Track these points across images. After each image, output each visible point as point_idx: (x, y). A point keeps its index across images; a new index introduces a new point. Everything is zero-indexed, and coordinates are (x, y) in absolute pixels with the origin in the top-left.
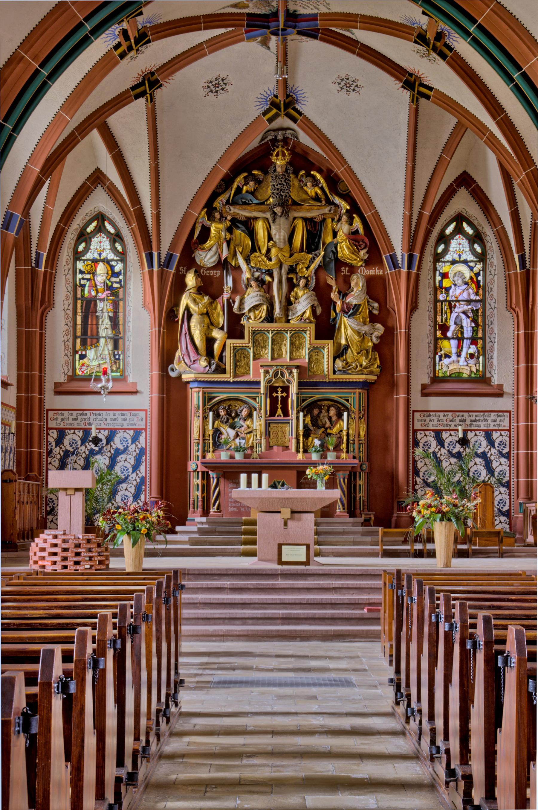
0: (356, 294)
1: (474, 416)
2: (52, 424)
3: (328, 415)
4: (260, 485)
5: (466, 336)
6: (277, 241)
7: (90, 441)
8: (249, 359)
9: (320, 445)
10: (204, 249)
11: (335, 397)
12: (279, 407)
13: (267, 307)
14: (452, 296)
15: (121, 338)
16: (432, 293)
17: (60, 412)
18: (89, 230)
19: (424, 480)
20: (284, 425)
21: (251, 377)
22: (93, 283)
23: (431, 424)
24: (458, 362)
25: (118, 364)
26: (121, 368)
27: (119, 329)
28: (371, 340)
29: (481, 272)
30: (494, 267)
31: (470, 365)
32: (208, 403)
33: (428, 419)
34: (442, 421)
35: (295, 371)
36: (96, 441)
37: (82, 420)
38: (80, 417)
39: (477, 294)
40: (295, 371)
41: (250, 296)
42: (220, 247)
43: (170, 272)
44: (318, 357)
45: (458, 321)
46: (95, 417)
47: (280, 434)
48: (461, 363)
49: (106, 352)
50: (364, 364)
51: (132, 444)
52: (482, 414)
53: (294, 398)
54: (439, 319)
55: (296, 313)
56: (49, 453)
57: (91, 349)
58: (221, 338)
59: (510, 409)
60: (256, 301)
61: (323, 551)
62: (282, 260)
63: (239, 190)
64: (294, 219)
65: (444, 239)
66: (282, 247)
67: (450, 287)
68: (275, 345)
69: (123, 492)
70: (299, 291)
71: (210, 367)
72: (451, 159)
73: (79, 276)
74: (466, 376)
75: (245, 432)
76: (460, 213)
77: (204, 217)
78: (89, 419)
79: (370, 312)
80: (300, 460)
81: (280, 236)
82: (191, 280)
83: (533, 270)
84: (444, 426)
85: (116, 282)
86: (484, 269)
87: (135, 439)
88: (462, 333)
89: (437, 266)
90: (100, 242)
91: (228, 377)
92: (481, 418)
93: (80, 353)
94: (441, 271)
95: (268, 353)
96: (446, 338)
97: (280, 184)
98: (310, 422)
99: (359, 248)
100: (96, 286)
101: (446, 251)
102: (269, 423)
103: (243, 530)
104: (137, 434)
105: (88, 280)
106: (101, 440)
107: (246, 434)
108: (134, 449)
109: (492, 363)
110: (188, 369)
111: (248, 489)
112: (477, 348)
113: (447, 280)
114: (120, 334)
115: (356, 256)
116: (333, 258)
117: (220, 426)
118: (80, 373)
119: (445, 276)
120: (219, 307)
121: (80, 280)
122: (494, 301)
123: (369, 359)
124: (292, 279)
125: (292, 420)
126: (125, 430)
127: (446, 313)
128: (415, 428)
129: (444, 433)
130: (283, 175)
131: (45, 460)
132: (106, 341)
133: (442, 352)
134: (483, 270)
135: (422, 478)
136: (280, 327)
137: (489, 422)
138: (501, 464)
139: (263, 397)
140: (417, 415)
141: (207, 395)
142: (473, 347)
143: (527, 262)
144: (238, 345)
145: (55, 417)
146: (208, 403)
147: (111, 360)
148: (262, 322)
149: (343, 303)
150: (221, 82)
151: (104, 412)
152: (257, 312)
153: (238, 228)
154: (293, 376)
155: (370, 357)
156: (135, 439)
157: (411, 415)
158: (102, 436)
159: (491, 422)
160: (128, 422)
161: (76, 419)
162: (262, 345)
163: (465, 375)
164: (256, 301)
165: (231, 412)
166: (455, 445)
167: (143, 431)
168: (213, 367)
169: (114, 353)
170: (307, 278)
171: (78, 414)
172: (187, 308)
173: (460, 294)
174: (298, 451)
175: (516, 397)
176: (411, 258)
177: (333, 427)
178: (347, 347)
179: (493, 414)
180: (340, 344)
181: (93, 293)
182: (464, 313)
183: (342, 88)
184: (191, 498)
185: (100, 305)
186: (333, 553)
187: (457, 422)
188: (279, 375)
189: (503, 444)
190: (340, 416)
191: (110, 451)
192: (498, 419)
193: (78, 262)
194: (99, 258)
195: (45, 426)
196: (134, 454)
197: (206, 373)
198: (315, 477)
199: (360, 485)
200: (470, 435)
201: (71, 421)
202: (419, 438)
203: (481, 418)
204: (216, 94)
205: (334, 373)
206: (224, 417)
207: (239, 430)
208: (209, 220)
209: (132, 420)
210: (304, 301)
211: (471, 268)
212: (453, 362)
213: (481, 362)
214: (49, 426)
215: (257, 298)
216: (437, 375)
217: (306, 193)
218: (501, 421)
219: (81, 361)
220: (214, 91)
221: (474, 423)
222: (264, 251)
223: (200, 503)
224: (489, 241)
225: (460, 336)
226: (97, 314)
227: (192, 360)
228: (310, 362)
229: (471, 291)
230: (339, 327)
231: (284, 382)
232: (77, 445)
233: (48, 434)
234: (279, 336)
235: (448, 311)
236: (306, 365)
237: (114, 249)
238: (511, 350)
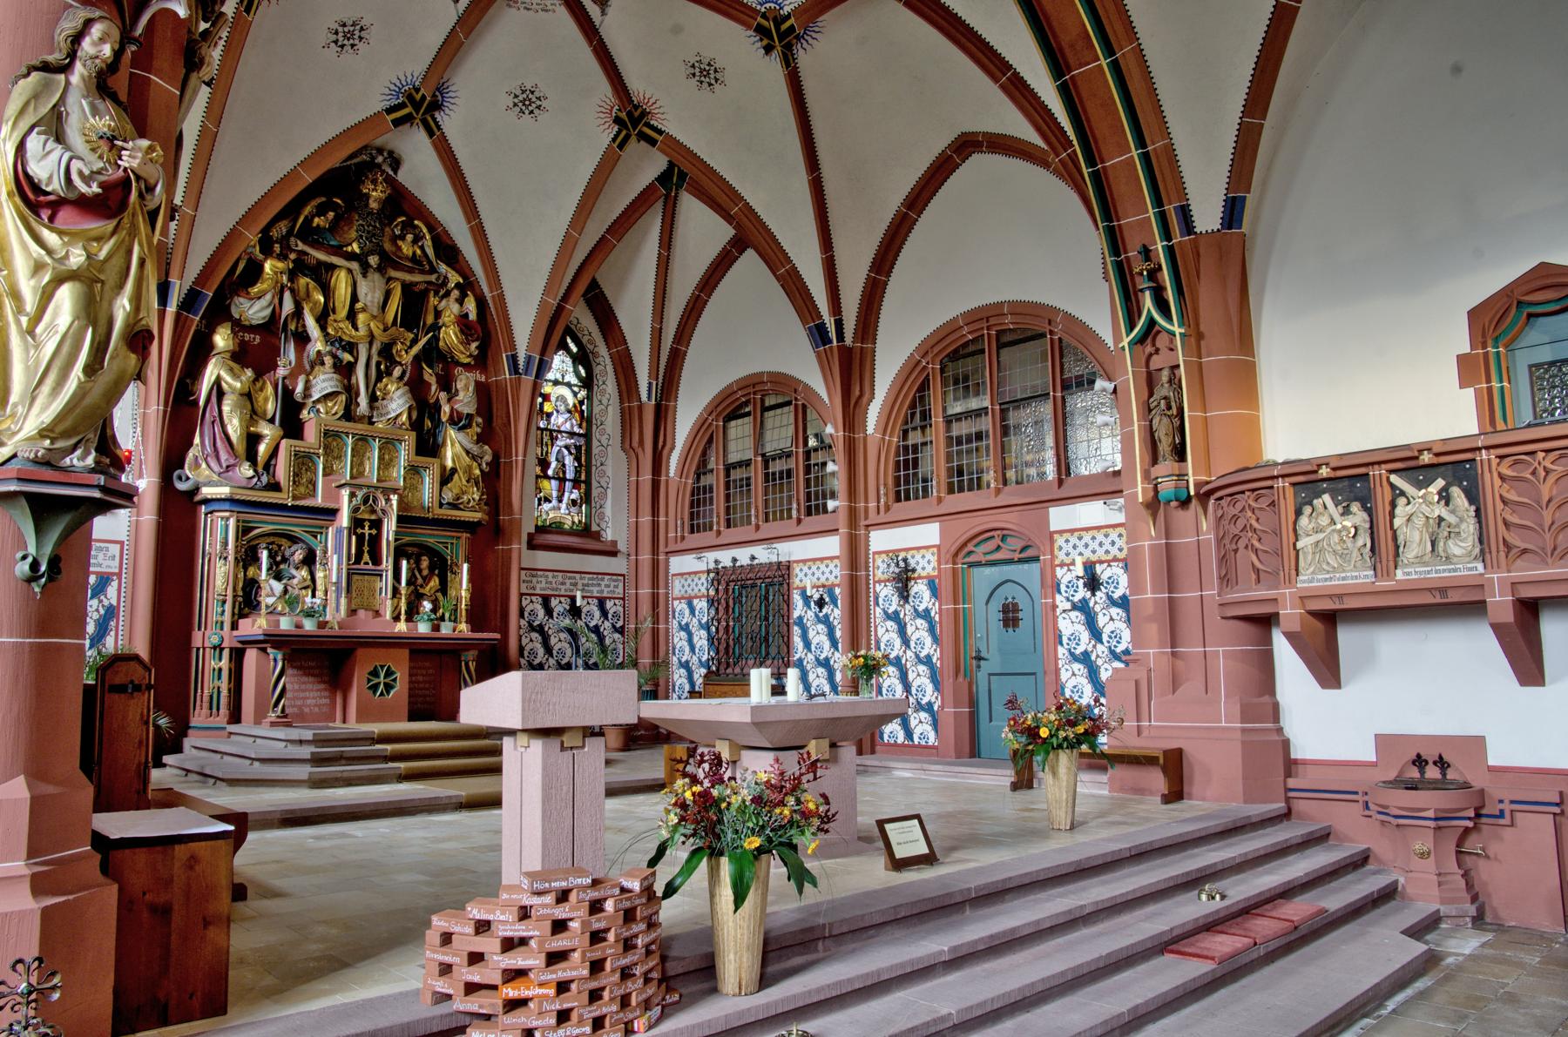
5: (568, 477)
9: (431, 611)
10: (248, 293)
21: (319, 501)
23: (538, 586)
32: (243, 536)
33: (534, 580)
34: (551, 583)
39: (580, 426)
43: (193, 320)
45: (560, 457)
48: (562, 511)
53: (390, 538)
55: (388, 413)
59: (624, 572)
66: (375, 314)
75: (300, 586)
77: (254, 247)
80: (400, 632)
81: (373, 297)
82: (222, 339)
84: (553, 589)
86: (589, 397)
88: (564, 473)
96: (547, 477)
103: (388, 754)
119: (546, 398)
127: (547, 445)
142: (575, 491)
144: (302, 449)
146: (243, 536)
148: (339, 419)
150: (357, 32)
154: (391, 505)
159: (605, 588)
163: (566, 526)
164: (331, 387)
167: (115, 578)
172: (218, 382)
178: (454, 471)
179: (607, 577)
182: (567, 447)
183: (515, 105)
184: (206, 691)
192: (613, 584)
197: (251, 489)
204: (339, 49)
205: (441, 505)
211: (575, 394)
215: (332, 383)
217: (399, 248)
218: (615, 587)
220: (340, 43)
223: (224, 701)
229: (574, 422)
235: (549, 442)
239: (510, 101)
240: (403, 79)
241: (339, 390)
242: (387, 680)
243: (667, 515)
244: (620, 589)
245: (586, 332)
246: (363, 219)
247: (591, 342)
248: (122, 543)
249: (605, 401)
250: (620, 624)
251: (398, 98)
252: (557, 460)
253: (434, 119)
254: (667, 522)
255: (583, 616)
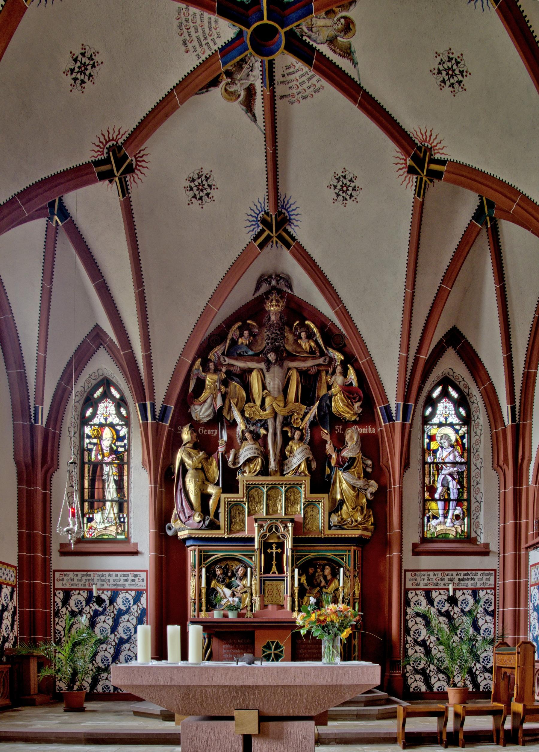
0: (351, 448)
1: (462, 575)
2: (58, 585)
3: (323, 574)
4: (184, 656)
5: (452, 497)
6: (272, 390)
7: (94, 602)
8: (245, 515)
9: (315, 603)
11: (330, 554)
12: (274, 564)
13: (262, 460)
14: (439, 458)
15: (125, 501)
16: (421, 454)
17: (65, 573)
18: (96, 396)
19: (414, 639)
20: (279, 583)
21: (246, 534)
22: (100, 448)
23: (422, 582)
24: (445, 523)
25: (123, 527)
26: (126, 530)
27: (124, 492)
28: (366, 495)
29: (466, 435)
30: (480, 427)
31: (456, 526)
32: (204, 561)
33: (418, 578)
34: (432, 580)
35: (290, 525)
36: (100, 601)
37: (86, 580)
38: (84, 578)
39: (462, 456)
40: (290, 525)
41: (245, 449)
42: (215, 398)
43: (165, 426)
44: (313, 513)
45: (445, 483)
46: (99, 578)
47: (274, 593)
48: (448, 525)
49: (112, 515)
50: (359, 519)
51: (133, 605)
52: (469, 572)
54: (427, 480)
55: (291, 467)
56: (57, 614)
57: (98, 512)
58: (216, 492)
59: (495, 567)
60: (250, 454)
61: (323, 737)
62: (276, 410)
63: (234, 342)
64: (289, 369)
65: (431, 402)
66: (276, 396)
67: (437, 450)
68: (270, 500)
69: (126, 652)
70: (293, 446)
71: (204, 523)
72: (451, 288)
73: (87, 441)
74: (453, 537)
75: (241, 592)
76: (446, 376)
78: (93, 580)
79: (364, 470)
81: (274, 384)
82: (186, 435)
83: (523, 424)
84: (433, 585)
85: (121, 446)
86: (469, 432)
87: (137, 600)
88: (449, 495)
89: (425, 429)
90: (106, 407)
91: (222, 533)
92: (469, 577)
93: (87, 516)
94: (429, 434)
95: (263, 508)
96: (434, 500)
97: (274, 333)
98: (305, 581)
99: (354, 401)
100: (102, 450)
101: (433, 414)
102: (264, 580)
104: (139, 594)
105: (95, 444)
106: (104, 601)
107: (242, 593)
108: (136, 610)
109: (478, 522)
110: (183, 526)
111: (155, 663)
112: (462, 509)
113: (435, 442)
114: (125, 497)
115: (350, 409)
116: (327, 412)
117: (217, 586)
118: (88, 536)
119: (432, 438)
120: (214, 462)
121: (87, 444)
122: (480, 460)
123: (364, 515)
124: (287, 432)
125: (287, 577)
126: (127, 590)
127: (434, 475)
128: (407, 587)
129: (434, 592)
130: (277, 323)
131: (52, 620)
132: (112, 505)
133: (430, 514)
134: (467, 433)
135: (412, 636)
136: (275, 481)
137: (476, 580)
138: (486, 622)
139: (257, 553)
140: (408, 574)
141: (203, 554)
143: (517, 416)
144: (232, 500)
145: (61, 578)
146: (204, 561)
147: (117, 523)
148: (257, 475)
149: (338, 456)
151: (107, 573)
152: (252, 466)
153: (233, 380)
154: (288, 531)
155: (365, 513)
156: (137, 600)
157: (403, 574)
158: (105, 596)
159: (478, 581)
160: (129, 582)
161: (81, 580)
162: (257, 500)
163: (451, 536)
164: (250, 454)
165: (228, 572)
166: (444, 604)
167: (144, 592)
168: (207, 522)
169: (119, 516)
170: (301, 430)
171: (82, 575)
172: (182, 463)
173: (447, 456)
174: (293, 610)
175: (502, 555)
176: (406, 408)
177: (329, 586)
178: (342, 502)
179: (479, 573)
180: (336, 499)
181: (100, 457)
182: (451, 475)
185: (106, 469)
186: (336, 739)
187: (446, 581)
188: (274, 529)
189: (488, 602)
190: (335, 574)
191: (113, 612)
193: (86, 427)
194: (105, 423)
195: (52, 587)
196: (136, 614)
197: (200, 529)
198: (317, 633)
199: (354, 645)
200: (459, 594)
201: (75, 582)
202: (410, 597)
203: (469, 577)
204: (200, 202)
205: (330, 528)
206: (221, 576)
207: (236, 590)
208: (203, 371)
209: (134, 580)
210: (298, 454)
211: (457, 431)
212: (440, 523)
213: (466, 523)
214: (56, 587)
215: (251, 451)
216: (425, 536)
217: (300, 346)
219: (89, 524)
220: (198, 197)
221: (462, 582)
222: (258, 402)
224: (475, 401)
225: (446, 497)
226: (104, 478)
227: (187, 516)
228: (305, 518)
229: (456, 454)
230: (334, 482)
231: (278, 538)
232: (82, 606)
233: (55, 595)
234: (274, 491)
235: (436, 473)
236: (302, 521)
237: (119, 414)
238: (496, 509)
239: (332, 193)
240: (254, 208)
241: (256, 455)
242: (276, 652)
243: (527, 518)
244: (492, 581)
245: (461, 379)
246: (268, 330)
247: (466, 386)
248: (146, 571)
249: (478, 433)
250: (491, 608)
251: (258, 226)
252: (442, 485)
253: (289, 234)
254: (527, 523)
255: (459, 603)
